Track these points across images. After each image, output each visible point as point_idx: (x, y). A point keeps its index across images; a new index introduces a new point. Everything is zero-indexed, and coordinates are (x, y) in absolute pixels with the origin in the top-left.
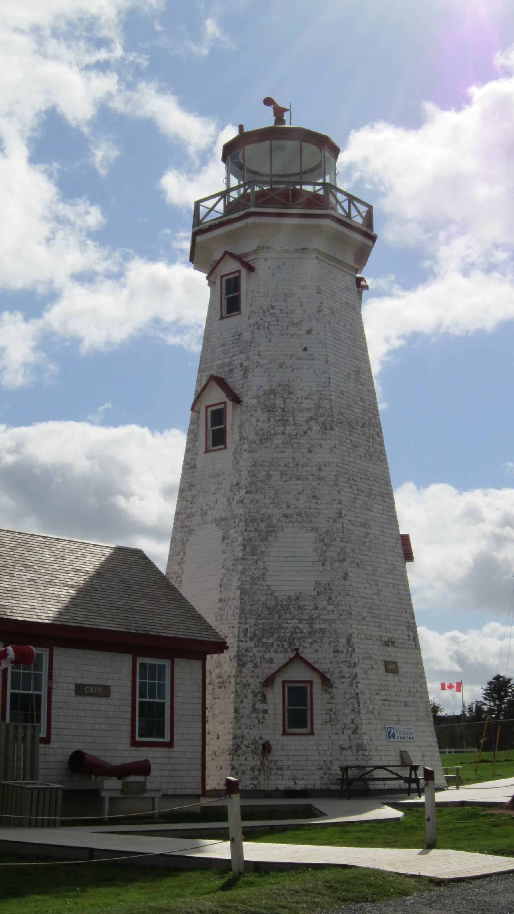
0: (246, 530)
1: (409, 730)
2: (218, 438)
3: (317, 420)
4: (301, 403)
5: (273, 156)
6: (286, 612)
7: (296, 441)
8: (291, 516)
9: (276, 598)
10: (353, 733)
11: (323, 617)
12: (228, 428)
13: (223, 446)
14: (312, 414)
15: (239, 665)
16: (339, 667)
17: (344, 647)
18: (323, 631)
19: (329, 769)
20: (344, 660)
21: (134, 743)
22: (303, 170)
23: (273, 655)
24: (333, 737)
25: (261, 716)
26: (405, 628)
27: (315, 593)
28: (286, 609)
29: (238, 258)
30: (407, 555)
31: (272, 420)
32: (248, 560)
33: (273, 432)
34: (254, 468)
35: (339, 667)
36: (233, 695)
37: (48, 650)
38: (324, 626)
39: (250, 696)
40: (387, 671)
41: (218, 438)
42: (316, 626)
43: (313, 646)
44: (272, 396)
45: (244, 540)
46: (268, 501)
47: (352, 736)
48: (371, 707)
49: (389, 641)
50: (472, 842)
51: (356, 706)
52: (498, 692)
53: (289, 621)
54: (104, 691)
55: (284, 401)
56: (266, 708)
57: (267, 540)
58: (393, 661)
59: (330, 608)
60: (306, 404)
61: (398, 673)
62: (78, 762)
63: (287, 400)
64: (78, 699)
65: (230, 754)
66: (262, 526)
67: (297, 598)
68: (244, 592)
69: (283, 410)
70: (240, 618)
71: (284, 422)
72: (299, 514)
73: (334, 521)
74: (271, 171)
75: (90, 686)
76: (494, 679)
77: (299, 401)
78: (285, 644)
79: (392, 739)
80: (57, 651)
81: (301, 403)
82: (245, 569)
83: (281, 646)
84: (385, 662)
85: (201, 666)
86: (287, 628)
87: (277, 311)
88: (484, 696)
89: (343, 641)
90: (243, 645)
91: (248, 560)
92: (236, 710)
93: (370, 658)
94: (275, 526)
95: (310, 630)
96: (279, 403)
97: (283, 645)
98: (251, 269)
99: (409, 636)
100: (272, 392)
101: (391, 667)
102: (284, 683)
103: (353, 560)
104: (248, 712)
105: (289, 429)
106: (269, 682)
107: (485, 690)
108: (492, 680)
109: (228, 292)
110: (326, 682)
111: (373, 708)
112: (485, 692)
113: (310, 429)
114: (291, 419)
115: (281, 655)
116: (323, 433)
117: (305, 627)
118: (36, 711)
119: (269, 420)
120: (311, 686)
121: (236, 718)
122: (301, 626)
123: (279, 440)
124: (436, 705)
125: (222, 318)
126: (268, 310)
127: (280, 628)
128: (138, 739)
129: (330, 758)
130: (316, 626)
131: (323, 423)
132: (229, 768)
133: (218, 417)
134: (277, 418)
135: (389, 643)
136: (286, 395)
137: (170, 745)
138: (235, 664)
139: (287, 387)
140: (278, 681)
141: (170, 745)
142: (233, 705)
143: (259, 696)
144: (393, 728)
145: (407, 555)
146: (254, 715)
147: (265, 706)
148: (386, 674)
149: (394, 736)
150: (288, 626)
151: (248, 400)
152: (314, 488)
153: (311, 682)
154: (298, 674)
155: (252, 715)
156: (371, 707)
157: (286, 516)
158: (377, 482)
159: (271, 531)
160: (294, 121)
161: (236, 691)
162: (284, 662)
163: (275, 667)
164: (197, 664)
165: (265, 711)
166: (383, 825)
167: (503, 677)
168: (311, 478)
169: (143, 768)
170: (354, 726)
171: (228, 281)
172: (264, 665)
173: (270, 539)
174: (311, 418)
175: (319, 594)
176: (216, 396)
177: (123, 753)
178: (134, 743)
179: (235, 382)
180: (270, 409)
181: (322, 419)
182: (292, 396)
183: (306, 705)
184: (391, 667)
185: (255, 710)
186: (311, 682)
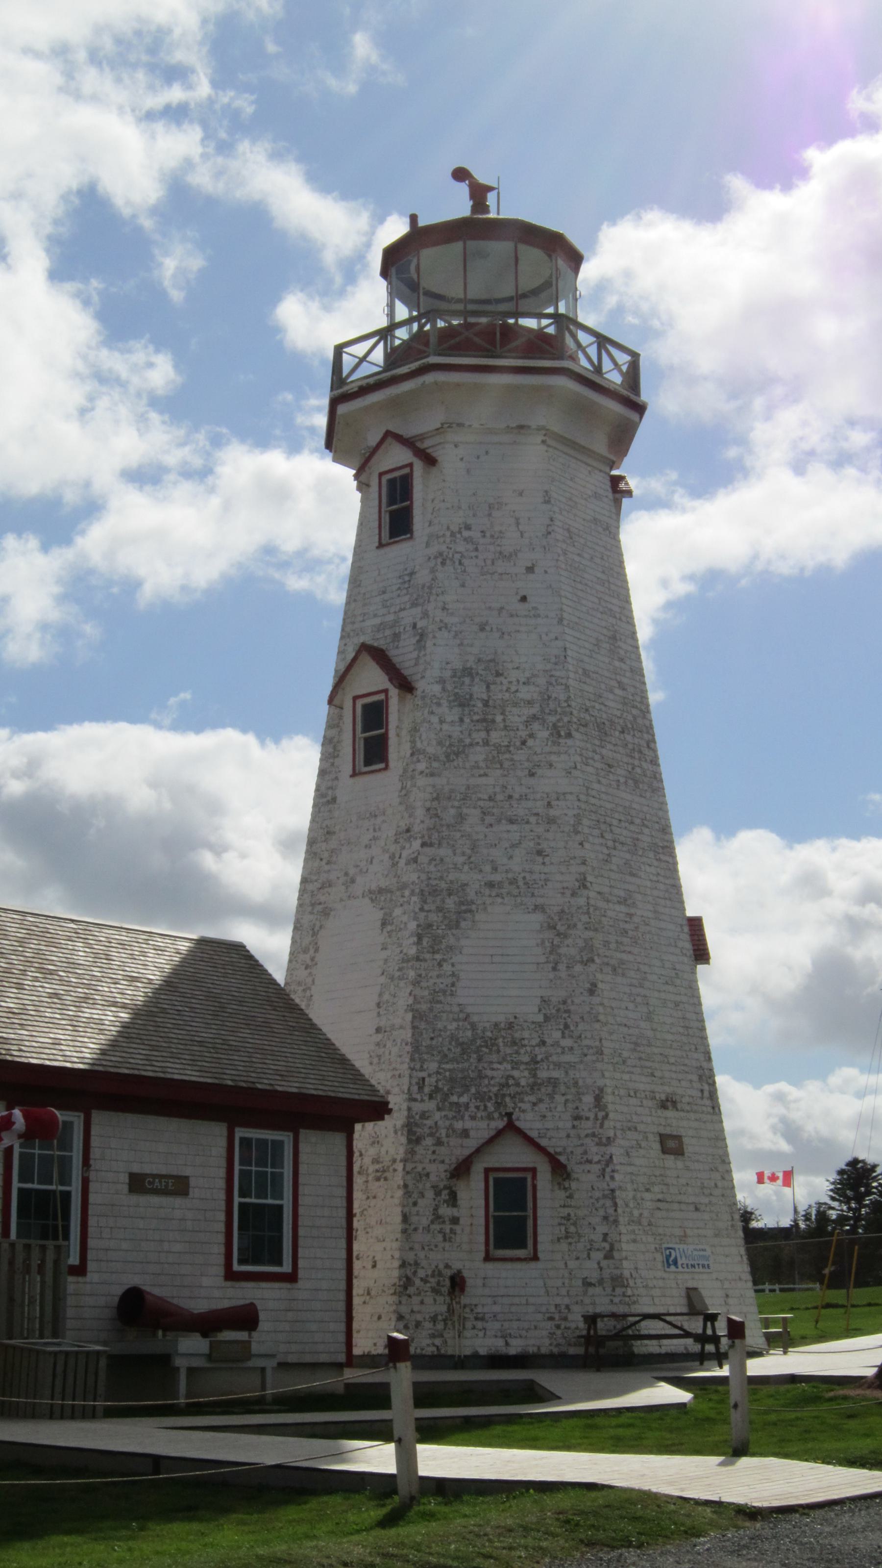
0: (422, 909)
1: (702, 1253)
2: (375, 752)
3: (544, 721)
4: (517, 691)
5: (468, 268)
6: (491, 1050)
7: (507, 756)
8: (500, 884)
9: (473, 1026)
10: (606, 1257)
11: (554, 1058)
12: (392, 734)
13: (382, 766)
14: (535, 710)
15: (410, 1141)
16: (582, 1145)
17: (590, 1110)
18: (554, 1083)
19: (565, 1319)
20: (590, 1131)
21: (230, 1275)
22: (520, 292)
23: (469, 1124)
24: (572, 1264)
25: (447, 1227)
26: (695, 1078)
27: (540, 1018)
28: (491, 1044)
29: (408, 442)
30: (698, 953)
31: (467, 720)
32: (425, 960)
33: (468, 741)
34: (436, 802)
35: (582, 1145)
36: (399, 1193)
37: (82, 1115)
38: (555, 1074)
39: (430, 1194)
40: (665, 1151)
41: (375, 752)
42: (543, 1074)
43: (536, 1108)
44: (467, 680)
45: (418, 926)
46: (461, 859)
47: (604, 1263)
48: (636, 1213)
49: (667, 1100)
50: (810, 1445)
51: (611, 1211)
52: (854, 1187)
53: (495, 1066)
54: (179, 1186)
55: (488, 687)
56: (456, 1214)
57: (458, 926)
58: (675, 1133)
59: (567, 1043)
60: (525, 693)
61: (683, 1154)
62: (135, 1308)
63: (492, 687)
64: (135, 1199)
65: (395, 1294)
66: (450, 903)
67: (510, 1026)
68: (418, 1016)
69: (486, 704)
70: (412, 1059)
71: (487, 724)
72: (513, 882)
73: (574, 894)
74: (465, 293)
75: (154, 1176)
76: (848, 1164)
77: (513, 688)
78: (489, 1105)
79: (673, 1268)
80: (97, 1117)
81: (517, 691)
82: (420, 976)
83: (482, 1108)
84: (661, 1135)
85: (345, 1143)
86: (492, 1078)
87: (475, 534)
88: (831, 1193)
89: (588, 1099)
90: (417, 1107)
91: (425, 960)
92: (405, 1218)
93: (636, 1129)
94: (472, 902)
95: (531, 1080)
96: (479, 691)
97: (485, 1107)
98: (430, 461)
99: (702, 1091)
100: (468, 672)
101: (671, 1145)
102: (487, 1171)
103: (606, 960)
104: (425, 1222)
105: (496, 737)
106: (461, 1170)
107: (833, 1183)
108: (844, 1167)
109: (392, 501)
110: (559, 1170)
111: (641, 1215)
112: (832, 1187)
113: (531, 736)
114: (499, 718)
115: (483, 1124)
116: (554, 743)
117: (523, 1076)
118: (63, 1220)
119: (461, 720)
120: (534, 1177)
121: (404, 1231)
122: (516, 1073)
123: (478, 755)
124: (749, 1210)
125: (381, 545)
126: (460, 532)
127: (481, 1077)
128: (236, 1267)
129: (567, 1301)
130: (543, 1074)
131: (555, 726)
132: (394, 1317)
133: (374, 715)
134: (476, 718)
135: (668, 1103)
136: (490, 678)
137: (292, 1278)
138: (404, 1140)
139: (492, 664)
140: (478, 1169)
141: (292, 1278)
142: (399, 1209)
143: (445, 1195)
144: (674, 1249)
145: (698, 953)
146: (436, 1227)
147: (454, 1212)
148: (663, 1156)
149: (675, 1263)
150: (495, 1073)
151: (426, 685)
152: (539, 837)
153: (534, 1171)
154: (512, 1156)
155: (433, 1227)
156: (636, 1213)
157: (491, 885)
158: (647, 827)
159: (465, 912)
160: (504, 207)
161: (406, 1186)
162: (487, 1135)
163: (472, 1144)
164: (337, 1140)
165: (455, 1221)
166: (657, 1415)
167: (863, 1161)
168: (533, 819)
169: (246, 1318)
170: (607, 1246)
171: (392, 482)
172: (454, 1141)
173: (463, 924)
174: (534, 717)
175: (547, 1018)
176: (371, 679)
177: (211, 1293)
178: (230, 1275)
179: (404, 655)
180: (463, 702)
181: (552, 719)
182: (502, 679)
183: (524, 1209)
184: (671, 1144)
185: (437, 1218)
186: (534, 1171)
